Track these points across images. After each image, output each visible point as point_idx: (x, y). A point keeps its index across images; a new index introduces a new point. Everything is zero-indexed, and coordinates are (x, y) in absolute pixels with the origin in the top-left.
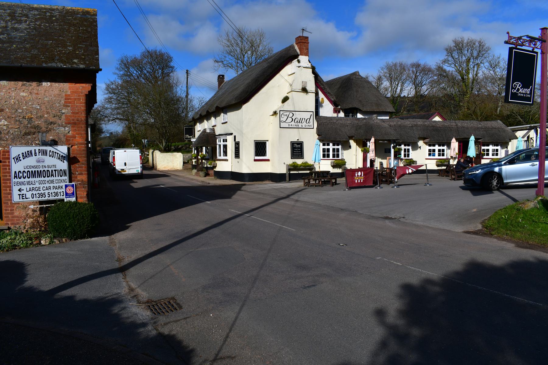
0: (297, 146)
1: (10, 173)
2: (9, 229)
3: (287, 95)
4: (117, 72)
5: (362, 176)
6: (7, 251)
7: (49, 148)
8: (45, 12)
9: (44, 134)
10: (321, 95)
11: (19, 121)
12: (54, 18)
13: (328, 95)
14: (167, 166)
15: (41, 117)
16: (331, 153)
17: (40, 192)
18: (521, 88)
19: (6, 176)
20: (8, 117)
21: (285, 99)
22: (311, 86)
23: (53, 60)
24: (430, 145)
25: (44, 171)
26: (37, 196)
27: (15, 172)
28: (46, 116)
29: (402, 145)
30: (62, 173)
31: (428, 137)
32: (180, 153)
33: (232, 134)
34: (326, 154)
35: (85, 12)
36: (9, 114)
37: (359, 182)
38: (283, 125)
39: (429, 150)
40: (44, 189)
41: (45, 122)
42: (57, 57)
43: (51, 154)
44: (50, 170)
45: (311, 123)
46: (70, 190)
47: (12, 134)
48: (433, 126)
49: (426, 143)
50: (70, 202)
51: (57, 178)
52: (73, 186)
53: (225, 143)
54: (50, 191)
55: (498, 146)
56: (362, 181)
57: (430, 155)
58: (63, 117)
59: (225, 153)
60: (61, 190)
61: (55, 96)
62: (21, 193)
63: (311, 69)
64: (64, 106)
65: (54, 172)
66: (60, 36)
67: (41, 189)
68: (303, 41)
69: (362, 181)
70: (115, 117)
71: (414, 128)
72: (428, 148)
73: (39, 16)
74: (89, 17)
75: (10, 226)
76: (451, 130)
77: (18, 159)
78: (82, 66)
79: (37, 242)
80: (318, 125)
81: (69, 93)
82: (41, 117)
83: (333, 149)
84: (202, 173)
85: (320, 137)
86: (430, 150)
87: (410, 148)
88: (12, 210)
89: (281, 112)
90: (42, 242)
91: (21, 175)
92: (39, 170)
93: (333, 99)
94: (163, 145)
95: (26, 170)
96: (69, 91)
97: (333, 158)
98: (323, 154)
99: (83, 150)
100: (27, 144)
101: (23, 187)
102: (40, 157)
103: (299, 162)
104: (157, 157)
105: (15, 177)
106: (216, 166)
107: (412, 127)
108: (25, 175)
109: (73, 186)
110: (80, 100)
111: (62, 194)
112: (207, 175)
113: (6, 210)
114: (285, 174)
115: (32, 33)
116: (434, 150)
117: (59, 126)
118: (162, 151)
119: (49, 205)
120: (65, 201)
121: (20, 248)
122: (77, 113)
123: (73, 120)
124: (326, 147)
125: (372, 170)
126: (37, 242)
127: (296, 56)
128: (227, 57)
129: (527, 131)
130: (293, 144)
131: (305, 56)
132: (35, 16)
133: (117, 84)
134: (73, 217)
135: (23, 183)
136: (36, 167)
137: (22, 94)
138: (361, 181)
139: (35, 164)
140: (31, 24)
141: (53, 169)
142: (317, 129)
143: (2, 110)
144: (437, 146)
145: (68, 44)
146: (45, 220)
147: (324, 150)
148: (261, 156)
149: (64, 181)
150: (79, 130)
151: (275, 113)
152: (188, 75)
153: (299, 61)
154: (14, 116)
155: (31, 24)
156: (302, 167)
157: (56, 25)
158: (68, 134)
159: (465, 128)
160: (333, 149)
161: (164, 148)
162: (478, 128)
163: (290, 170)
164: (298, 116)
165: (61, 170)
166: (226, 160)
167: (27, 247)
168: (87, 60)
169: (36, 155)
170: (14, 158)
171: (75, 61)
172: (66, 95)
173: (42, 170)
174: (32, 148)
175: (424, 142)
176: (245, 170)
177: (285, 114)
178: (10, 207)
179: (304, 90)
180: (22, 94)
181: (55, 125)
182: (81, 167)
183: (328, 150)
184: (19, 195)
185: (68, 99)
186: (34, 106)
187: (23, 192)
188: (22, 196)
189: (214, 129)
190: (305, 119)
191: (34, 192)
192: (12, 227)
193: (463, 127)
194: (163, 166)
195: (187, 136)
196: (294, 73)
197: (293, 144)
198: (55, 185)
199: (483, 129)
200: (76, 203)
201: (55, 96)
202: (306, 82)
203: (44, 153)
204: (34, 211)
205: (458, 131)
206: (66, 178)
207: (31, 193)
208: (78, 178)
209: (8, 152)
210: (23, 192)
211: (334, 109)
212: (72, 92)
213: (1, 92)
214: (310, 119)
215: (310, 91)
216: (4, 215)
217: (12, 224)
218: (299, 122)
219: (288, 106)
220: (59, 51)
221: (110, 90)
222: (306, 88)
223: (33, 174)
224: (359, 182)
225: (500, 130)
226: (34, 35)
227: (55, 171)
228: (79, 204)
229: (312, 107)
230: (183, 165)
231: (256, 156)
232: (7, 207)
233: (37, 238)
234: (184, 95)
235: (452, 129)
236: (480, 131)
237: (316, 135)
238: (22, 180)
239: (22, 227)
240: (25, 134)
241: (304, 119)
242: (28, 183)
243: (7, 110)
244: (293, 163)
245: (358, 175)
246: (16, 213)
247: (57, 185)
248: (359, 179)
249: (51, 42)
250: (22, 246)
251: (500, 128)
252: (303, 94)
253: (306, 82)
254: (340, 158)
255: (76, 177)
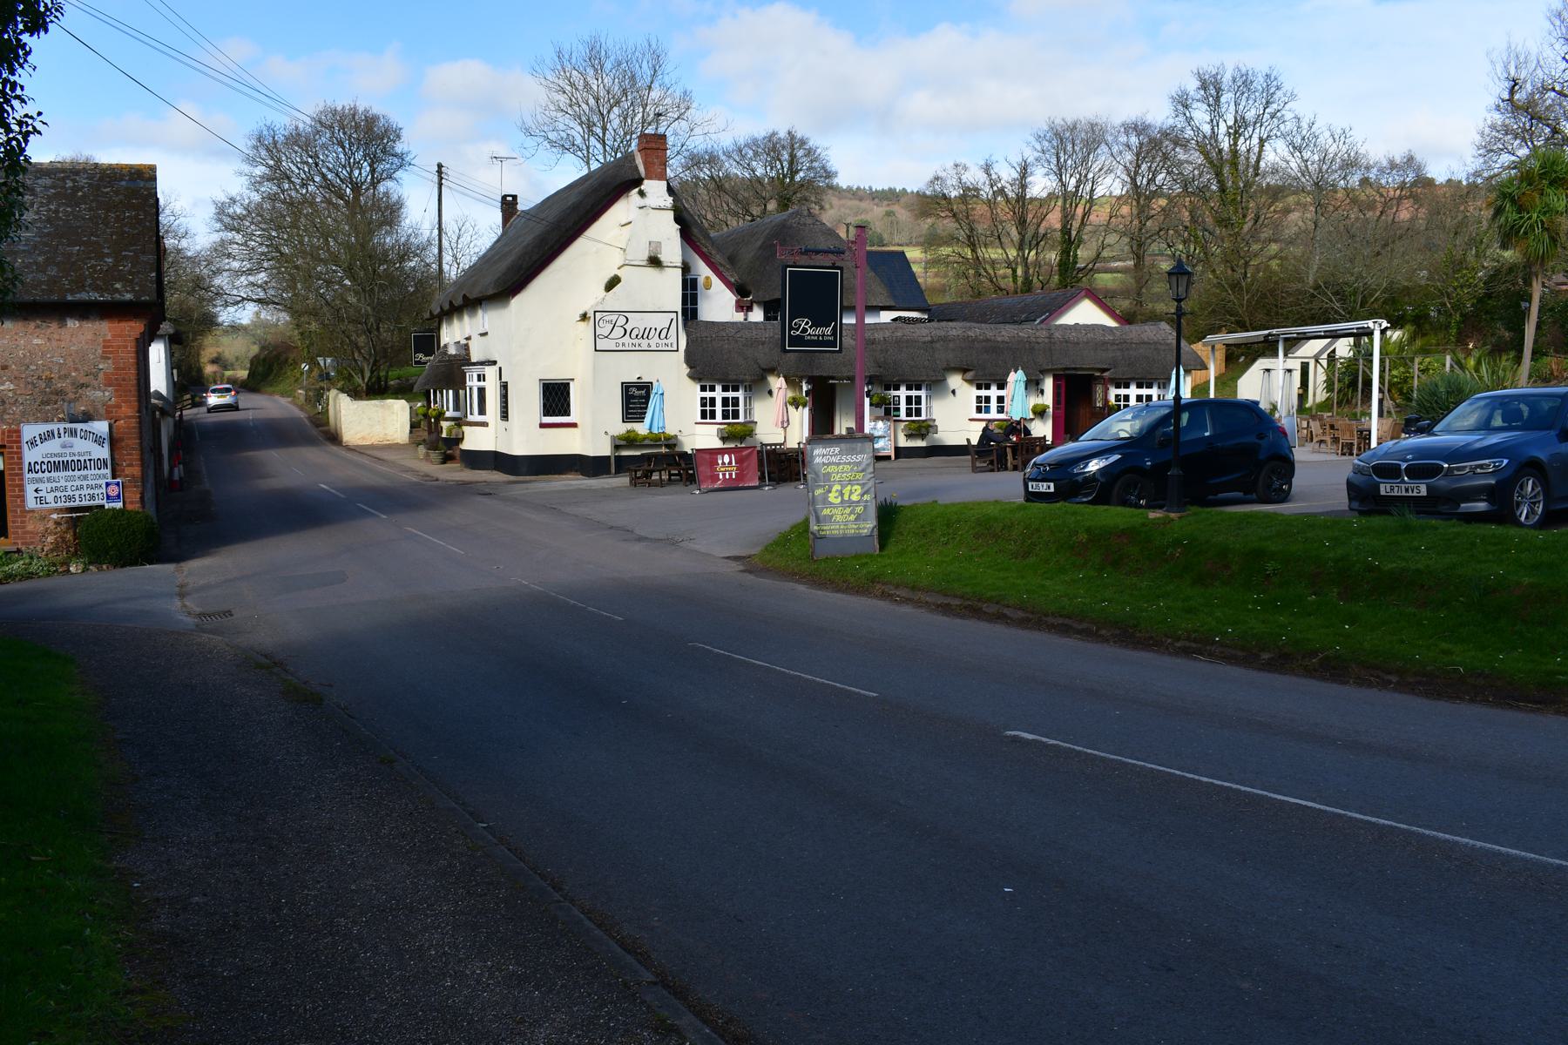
0: (637, 393)
1: (21, 464)
2: (19, 551)
3: (619, 273)
4: (246, 168)
5: (734, 464)
6: (20, 580)
7: (79, 426)
8: (63, 179)
9: (72, 405)
10: (703, 271)
11: (33, 383)
12: (80, 194)
13: (721, 269)
14: (369, 434)
15: (66, 376)
16: (719, 408)
17: (67, 494)
18: (811, 327)
19: (13, 469)
20: (15, 378)
21: (613, 283)
22: (673, 250)
23: (82, 288)
24: (979, 387)
25: (73, 460)
26: (63, 499)
27: (30, 463)
28: (73, 374)
29: (901, 388)
30: (100, 464)
31: (971, 368)
32: (403, 401)
33: (494, 363)
34: (707, 414)
35: (134, 173)
36: (16, 373)
37: (727, 477)
38: (602, 344)
39: (977, 397)
40: (73, 488)
41: (73, 384)
42: (89, 281)
43: (83, 434)
44: (82, 459)
45: (673, 339)
46: (114, 491)
47: (22, 403)
48: (988, 340)
49: (970, 382)
50: (114, 509)
51: (93, 472)
52: (118, 484)
53: (482, 384)
54: (83, 492)
55: (1152, 388)
56: (734, 477)
57: (979, 410)
58: (101, 375)
59: (482, 411)
60: (99, 491)
61: (87, 343)
62: (38, 495)
63: (672, 212)
64: (102, 358)
65: (88, 462)
66: (92, 235)
67: (69, 489)
68: (654, 146)
69: (734, 477)
70: (242, 294)
71: (938, 345)
72: (975, 392)
73: (53, 191)
74: (142, 184)
75: (20, 547)
76: (1032, 349)
77: (33, 443)
78: (128, 296)
79: (65, 568)
80: (688, 343)
81: (109, 337)
82: (66, 376)
83: (723, 398)
84: (435, 455)
85: (693, 370)
86: (979, 398)
87: (922, 393)
88: (23, 522)
89: (597, 313)
90: (71, 569)
91: (38, 467)
92: (65, 459)
93: (733, 280)
94: (363, 379)
95: (46, 460)
96: (110, 334)
97: (723, 419)
98: (702, 410)
99: (134, 428)
100: (46, 421)
101: (41, 486)
102: (66, 439)
103: (641, 429)
104: (343, 412)
105: (29, 471)
106: (463, 439)
107: (932, 342)
108: (44, 467)
109: (118, 484)
110: (127, 348)
111: (101, 496)
112: (447, 459)
113: (14, 522)
114: (608, 458)
115: (46, 231)
116: (988, 399)
117: (94, 389)
118: (355, 394)
119: (81, 514)
120: (106, 507)
121: (39, 577)
122: (124, 369)
123: (116, 379)
124: (708, 394)
125: (752, 451)
126: (65, 568)
127: (638, 182)
128: (560, 119)
129: (1329, 340)
130: (626, 387)
131: (657, 182)
132: (45, 190)
133: (247, 201)
134: (119, 532)
135: (40, 480)
136: (60, 455)
137: (36, 341)
138: (731, 475)
139: (58, 450)
140: (41, 209)
141: (87, 458)
142: (687, 351)
143: (5, 368)
144: (994, 388)
145: (106, 251)
146: (75, 536)
147: (703, 401)
148: (562, 415)
149: (105, 476)
150: (126, 396)
151: (584, 317)
152: (442, 178)
153: (642, 194)
154: (23, 376)
155: (41, 209)
156: (647, 442)
157: (84, 209)
158: (109, 403)
159: (1069, 344)
160: (723, 398)
161: (367, 385)
162: (1104, 343)
163: (617, 447)
164: (636, 322)
165: (99, 459)
166: (484, 424)
167: (48, 575)
168: (137, 283)
169: (60, 437)
170: (27, 442)
171: (118, 286)
172: (104, 341)
173: (70, 459)
174: (53, 427)
175: (964, 380)
176: (519, 449)
177: (607, 318)
178: (20, 517)
179: (655, 262)
180: (36, 341)
181: (89, 389)
182: (131, 454)
183: (713, 401)
184: (36, 498)
185: (109, 347)
186: (54, 359)
187: (41, 494)
188: (40, 500)
189: (467, 345)
190: (656, 329)
191: (58, 494)
192: (23, 548)
193: (1066, 342)
194: (359, 436)
195: (420, 355)
196: (631, 222)
197: (626, 387)
198: (90, 483)
199: (1117, 345)
200: (122, 511)
201: (87, 343)
202: (660, 243)
203: (73, 433)
204: (57, 523)
205: (1050, 350)
206: (108, 471)
207: (53, 494)
208: (127, 472)
209: (18, 432)
210: (41, 494)
211: (737, 302)
212: (113, 336)
213: (3, 338)
214: (668, 329)
215: (669, 265)
216: (10, 530)
217: (22, 544)
218: (642, 336)
219: (616, 299)
220: (91, 267)
221: (227, 220)
222: (659, 256)
223: (56, 466)
224: (727, 477)
225: (1159, 347)
226: (49, 234)
227: (90, 460)
228: (129, 512)
229: (673, 298)
230: (411, 432)
231: (544, 415)
232: (15, 517)
233: (62, 564)
234: (427, 230)
235: (1037, 346)
236: (1107, 349)
237: (685, 366)
238: (40, 475)
239: (39, 548)
240: (43, 404)
241: (653, 330)
242: (49, 480)
243: (13, 367)
244: (628, 432)
245: (723, 463)
246: (30, 527)
247: (93, 483)
248: (726, 471)
249: (78, 248)
250: (41, 574)
251: (1161, 344)
252: (652, 272)
253: (660, 243)
254: (741, 419)
255: (124, 470)
